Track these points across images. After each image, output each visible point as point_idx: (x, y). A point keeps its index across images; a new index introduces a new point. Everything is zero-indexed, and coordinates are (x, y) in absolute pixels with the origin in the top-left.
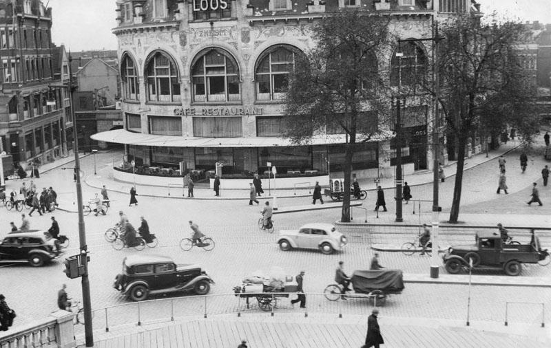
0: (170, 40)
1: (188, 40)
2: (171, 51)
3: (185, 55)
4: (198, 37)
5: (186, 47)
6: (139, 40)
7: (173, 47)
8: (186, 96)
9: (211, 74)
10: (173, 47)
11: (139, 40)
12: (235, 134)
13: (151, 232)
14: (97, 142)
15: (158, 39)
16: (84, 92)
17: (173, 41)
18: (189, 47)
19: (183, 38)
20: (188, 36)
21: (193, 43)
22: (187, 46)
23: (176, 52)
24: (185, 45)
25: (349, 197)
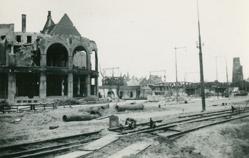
0: (65, 40)
1: (72, 42)
4: (76, 41)
5: (72, 45)
8: (71, 65)
9: (44, 61)
10: (66, 43)
15: (58, 39)
20: (72, 40)
22: (72, 44)
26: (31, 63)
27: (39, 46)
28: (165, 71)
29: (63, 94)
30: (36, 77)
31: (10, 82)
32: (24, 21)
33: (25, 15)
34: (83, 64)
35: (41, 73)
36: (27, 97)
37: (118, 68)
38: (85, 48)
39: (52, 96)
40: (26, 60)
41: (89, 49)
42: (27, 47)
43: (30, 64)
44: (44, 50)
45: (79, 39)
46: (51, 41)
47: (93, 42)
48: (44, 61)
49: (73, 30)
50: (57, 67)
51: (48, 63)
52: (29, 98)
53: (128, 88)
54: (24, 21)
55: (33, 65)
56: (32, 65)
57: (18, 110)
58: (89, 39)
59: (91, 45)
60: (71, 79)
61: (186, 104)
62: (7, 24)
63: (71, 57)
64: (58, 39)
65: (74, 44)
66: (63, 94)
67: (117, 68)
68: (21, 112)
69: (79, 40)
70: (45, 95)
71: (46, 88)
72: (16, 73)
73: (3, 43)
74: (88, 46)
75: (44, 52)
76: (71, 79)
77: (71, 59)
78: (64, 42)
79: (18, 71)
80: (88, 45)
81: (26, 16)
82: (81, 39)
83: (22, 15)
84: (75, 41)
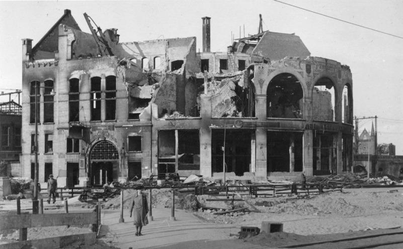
0: (298, 67)
1: (312, 70)
2: (298, 76)
3: (309, 81)
5: (310, 74)
6: (45, 209)
7: (300, 73)
8: (309, 114)
9: (261, 108)
10: (300, 73)
11: (45, 209)
12: (160, 139)
13: (62, 14)
14: (34, 48)
15: (286, 64)
16: (71, 214)
17: (300, 68)
18: (312, 75)
19: (308, 67)
20: (312, 66)
21: (315, 72)
22: (311, 74)
23: (303, 77)
24: (309, 73)
25: (318, 171)
26: (232, 112)
27: (252, 80)
28: (376, 117)
29: (291, 167)
30: (247, 135)
31: (204, 147)
32: (207, 30)
33: (209, 19)
34: (316, 110)
35: (258, 130)
36: (233, 173)
37: (376, 117)
38: (334, 80)
39: (277, 173)
40: (221, 105)
41: (340, 81)
42: (223, 80)
43: (229, 112)
44: (261, 87)
45: (323, 64)
46: (274, 68)
47: (347, 68)
48: (261, 108)
49: (296, 43)
50: (271, 118)
51: (270, 112)
52: (237, 174)
53: (395, 160)
54: (207, 30)
55: (235, 114)
56: (233, 115)
57: (274, 192)
58: (339, 63)
59: (343, 73)
60: (307, 142)
61: (139, 237)
62: (183, 39)
63: (261, 95)
64: (286, 64)
65: (314, 74)
66: (291, 167)
67: (372, 117)
68: (278, 197)
69: (323, 66)
70: (265, 169)
71: (266, 158)
72: (213, 130)
73: (180, 75)
74: (338, 76)
75: (261, 91)
76: (307, 142)
77: (309, 102)
78: (296, 70)
79: (217, 127)
80: (338, 74)
81: (211, 20)
82: (326, 64)
83: (204, 19)
84: (317, 68)
